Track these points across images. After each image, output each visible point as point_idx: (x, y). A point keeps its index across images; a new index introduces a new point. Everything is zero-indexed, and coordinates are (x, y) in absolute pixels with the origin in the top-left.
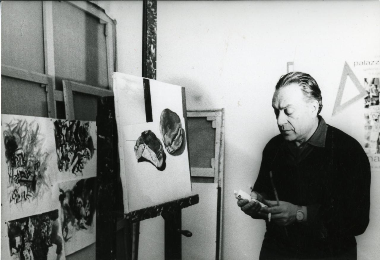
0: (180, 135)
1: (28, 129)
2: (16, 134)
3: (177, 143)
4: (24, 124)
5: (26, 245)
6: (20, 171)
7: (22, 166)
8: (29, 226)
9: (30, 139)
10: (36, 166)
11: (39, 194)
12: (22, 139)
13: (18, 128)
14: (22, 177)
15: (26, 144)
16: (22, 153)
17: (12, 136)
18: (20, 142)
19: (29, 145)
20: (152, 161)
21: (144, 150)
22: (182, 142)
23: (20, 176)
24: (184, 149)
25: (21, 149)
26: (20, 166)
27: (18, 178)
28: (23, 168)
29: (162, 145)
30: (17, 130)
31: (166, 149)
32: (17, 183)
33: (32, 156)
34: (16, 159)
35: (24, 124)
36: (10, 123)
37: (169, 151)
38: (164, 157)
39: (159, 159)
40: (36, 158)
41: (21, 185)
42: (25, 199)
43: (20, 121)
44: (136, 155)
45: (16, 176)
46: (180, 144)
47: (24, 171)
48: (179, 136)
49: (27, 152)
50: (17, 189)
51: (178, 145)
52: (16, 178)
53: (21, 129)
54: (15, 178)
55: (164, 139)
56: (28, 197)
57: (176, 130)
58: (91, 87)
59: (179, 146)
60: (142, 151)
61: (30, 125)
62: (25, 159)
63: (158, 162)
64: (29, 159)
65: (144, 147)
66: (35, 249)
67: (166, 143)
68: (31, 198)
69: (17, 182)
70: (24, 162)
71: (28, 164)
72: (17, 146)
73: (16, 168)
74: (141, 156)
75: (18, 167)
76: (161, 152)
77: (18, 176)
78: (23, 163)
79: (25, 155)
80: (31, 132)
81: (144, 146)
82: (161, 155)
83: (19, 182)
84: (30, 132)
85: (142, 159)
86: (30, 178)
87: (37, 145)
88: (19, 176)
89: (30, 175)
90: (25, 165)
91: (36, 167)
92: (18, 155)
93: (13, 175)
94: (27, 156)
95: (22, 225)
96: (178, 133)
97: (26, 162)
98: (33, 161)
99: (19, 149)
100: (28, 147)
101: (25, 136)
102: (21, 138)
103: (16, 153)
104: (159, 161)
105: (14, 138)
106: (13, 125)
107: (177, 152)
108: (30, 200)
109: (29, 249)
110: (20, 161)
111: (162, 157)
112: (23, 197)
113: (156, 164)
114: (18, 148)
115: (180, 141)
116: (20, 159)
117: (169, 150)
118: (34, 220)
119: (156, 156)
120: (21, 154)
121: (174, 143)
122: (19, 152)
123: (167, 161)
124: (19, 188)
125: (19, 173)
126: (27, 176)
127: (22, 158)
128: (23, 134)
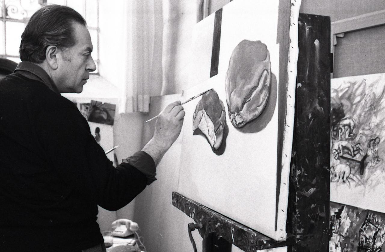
0: (264, 86)
1: (367, 92)
2: (346, 100)
3: (254, 106)
4: (359, 86)
5: (333, 235)
6: (342, 146)
7: (346, 140)
8: (341, 215)
9: (368, 105)
10: (372, 142)
11: (369, 182)
12: (354, 106)
13: (349, 92)
14: (344, 153)
15: (358, 112)
16: (350, 123)
17: (339, 103)
18: (350, 110)
19: (363, 114)
20: (207, 136)
21: (202, 118)
22: (264, 102)
23: (341, 151)
24: (270, 119)
25: (350, 118)
26: (344, 139)
27: (338, 154)
28: (348, 142)
29: (224, 111)
30: (347, 96)
31: (230, 118)
32: (336, 160)
33: (367, 128)
34: (340, 131)
35: (359, 86)
36: (338, 88)
37: (235, 123)
38: (226, 132)
39: (217, 135)
40: (373, 132)
41: (341, 163)
42: (344, 182)
43: (354, 84)
44: (193, 125)
45: (337, 151)
46: (260, 109)
47: (350, 146)
48: (261, 92)
49: (359, 123)
50: (334, 166)
51: (255, 109)
52: (336, 153)
53: (355, 93)
54: (335, 153)
55: (228, 101)
56: (350, 180)
57: (255, 78)
58: (346, 20)
59: (257, 113)
60: (200, 120)
61: (372, 86)
62: (354, 132)
63: (215, 140)
64: (361, 131)
65: (203, 115)
66: (345, 249)
67: (231, 108)
68: (353, 184)
69: (337, 158)
70: (352, 135)
71: (357, 139)
72: (344, 116)
73: (338, 141)
74: (197, 127)
75: (341, 140)
76: (222, 123)
77: (339, 151)
78: (349, 136)
79: (354, 127)
80: (372, 96)
81: (202, 113)
82: (221, 128)
83: (338, 159)
84: (370, 96)
85: (198, 132)
86: (358, 157)
87: (379, 114)
88: (340, 151)
89: (359, 153)
90: (352, 137)
91: (372, 145)
92: (344, 126)
93: (333, 149)
94: (358, 128)
95: (333, 211)
96: (258, 84)
97: (356, 135)
98: (366, 136)
99: (346, 119)
100: (362, 117)
101: (359, 102)
102: (352, 105)
103: (341, 123)
104: (217, 138)
105: (342, 105)
106: (342, 90)
107: (252, 125)
108: (351, 186)
109: (337, 243)
110: (344, 133)
111: (222, 131)
112: (341, 178)
113: (212, 142)
114: (345, 118)
115: (261, 100)
116: (344, 131)
117: (236, 121)
118: (353, 212)
119: (214, 129)
120: (349, 125)
121: (247, 106)
122: (346, 122)
123: (228, 141)
124: (337, 165)
125: (341, 147)
126: (353, 154)
127: (349, 129)
128: (358, 99)
